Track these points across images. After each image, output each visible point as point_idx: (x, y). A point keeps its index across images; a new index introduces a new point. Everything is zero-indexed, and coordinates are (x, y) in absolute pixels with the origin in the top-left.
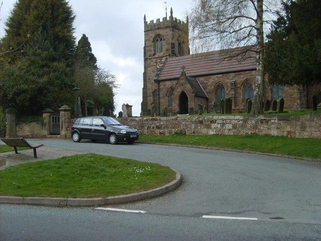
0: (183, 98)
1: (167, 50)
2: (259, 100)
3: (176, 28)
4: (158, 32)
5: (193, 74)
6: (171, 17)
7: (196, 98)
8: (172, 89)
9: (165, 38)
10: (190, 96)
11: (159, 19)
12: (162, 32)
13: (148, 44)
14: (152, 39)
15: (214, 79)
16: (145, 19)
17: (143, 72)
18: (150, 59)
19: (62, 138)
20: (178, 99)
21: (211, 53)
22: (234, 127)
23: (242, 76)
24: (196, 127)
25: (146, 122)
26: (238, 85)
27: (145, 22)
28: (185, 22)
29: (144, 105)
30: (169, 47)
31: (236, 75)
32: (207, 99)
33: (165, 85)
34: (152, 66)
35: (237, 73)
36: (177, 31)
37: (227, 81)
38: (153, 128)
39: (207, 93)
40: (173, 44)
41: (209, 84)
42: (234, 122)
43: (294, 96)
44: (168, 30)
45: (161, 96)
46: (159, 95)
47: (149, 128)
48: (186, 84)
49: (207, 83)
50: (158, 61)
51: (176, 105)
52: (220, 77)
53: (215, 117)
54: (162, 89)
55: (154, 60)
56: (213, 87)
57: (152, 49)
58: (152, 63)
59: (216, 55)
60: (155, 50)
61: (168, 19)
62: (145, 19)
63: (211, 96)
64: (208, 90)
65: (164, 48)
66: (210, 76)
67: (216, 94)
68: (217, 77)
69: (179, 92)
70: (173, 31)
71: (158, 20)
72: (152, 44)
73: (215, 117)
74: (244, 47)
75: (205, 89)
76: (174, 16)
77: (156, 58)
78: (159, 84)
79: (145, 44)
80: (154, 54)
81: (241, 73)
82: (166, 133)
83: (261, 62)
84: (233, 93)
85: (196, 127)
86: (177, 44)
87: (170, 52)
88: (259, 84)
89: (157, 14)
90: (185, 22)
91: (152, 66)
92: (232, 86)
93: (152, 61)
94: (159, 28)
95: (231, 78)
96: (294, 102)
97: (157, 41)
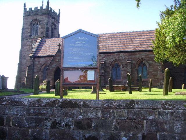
1: (42, 33)
4: (35, 17)
6: (48, 7)
11: (37, 8)
12: (38, 18)
13: (26, 26)
14: (29, 23)
16: (25, 6)
17: (20, 49)
23: (111, 57)
25: (49, 111)
26: (108, 65)
27: (25, 9)
28: (58, 13)
29: (19, 79)
33: (40, 61)
34: (28, 45)
36: (51, 18)
38: (67, 125)
40: (47, 28)
43: (157, 77)
44: (44, 16)
45: (35, 71)
46: (33, 70)
47: (55, 125)
50: (34, 41)
55: (30, 40)
57: (29, 31)
60: (31, 33)
61: (44, 8)
62: (25, 6)
65: (39, 32)
69: (54, 67)
70: (48, 17)
71: (36, 8)
72: (30, 27)
76: (50, 6)
79: (23, 26)
80: (30, 36)
81: (110, 54)
84: (103, 71)
86: (50, 29)
90: (58, 13)
93: (28, 41)
94: (36, 15)
96: (157, 82)
97: (34, 24)
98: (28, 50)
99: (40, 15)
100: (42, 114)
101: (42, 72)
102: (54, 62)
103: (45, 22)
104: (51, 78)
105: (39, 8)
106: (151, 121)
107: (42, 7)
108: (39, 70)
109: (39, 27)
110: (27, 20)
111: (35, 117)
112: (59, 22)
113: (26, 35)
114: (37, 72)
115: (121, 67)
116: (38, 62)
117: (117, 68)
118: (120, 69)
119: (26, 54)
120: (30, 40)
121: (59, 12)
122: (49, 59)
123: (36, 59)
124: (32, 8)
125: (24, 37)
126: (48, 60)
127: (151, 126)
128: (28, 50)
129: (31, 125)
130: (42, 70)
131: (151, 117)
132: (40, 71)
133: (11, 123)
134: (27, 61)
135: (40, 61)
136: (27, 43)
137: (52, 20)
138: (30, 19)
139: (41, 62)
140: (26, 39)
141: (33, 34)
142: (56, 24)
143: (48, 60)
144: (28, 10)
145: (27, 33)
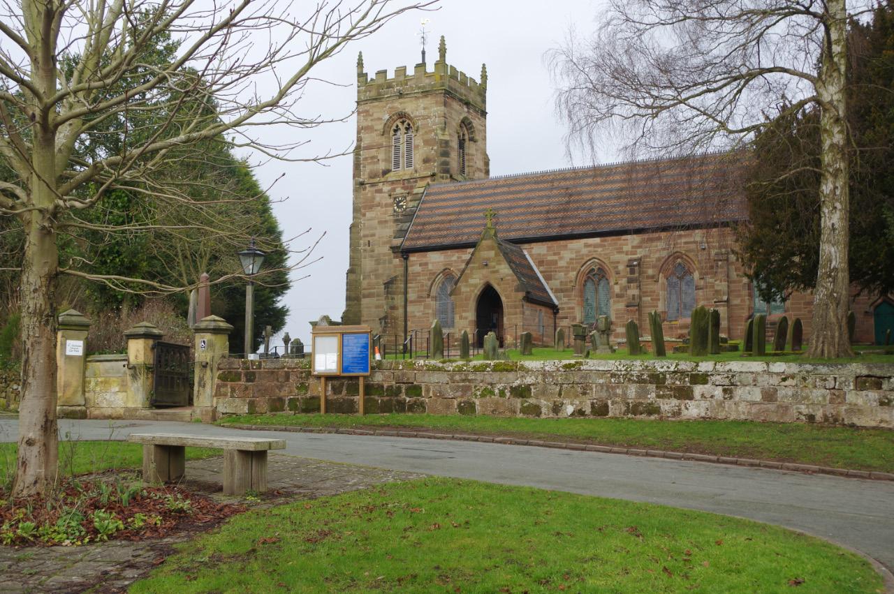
0: (489, 304)
1: (426, 161)
2: (836, 315)
3: (453, 98)
4: (399, 105)
5: (513, 235)
7: (526, 304)
8: (451, 279)
9: (420, 123)
10: (509, 297)
13: (368, 139)
15: (577, 252)
16: (360, 64)
17: (351, 222)
18: (373, 185)
19: (198, 421)
20: (472, 305)
21: (501, 183)
22: (769, 396)
23: (660, 245)
24: (643, 393)
25: (479, 376)
27: (362, 75)
28: (479, 81)
30: (433, 151)
31: (643, 241)
32: (554, 309)
33: (426, 264)
34: (379, 205)
35: (646, 236)
37: (616, 257)
38: (502, 393)
39: (556, 291)
41: (562, 263)
42: (766, 381)
46: (406, 293)
48: (499, 263)
49: (555, 262)
51: (465, 322)
52: (595, 246)
53: (705, 366)
54: (418, 274)
55: (386, 188)
56: (573, 274)
58: (378, 197)
59: (617, 177)
61: (430, 68)
62: (360, 64)
63: (565, 300)
64: (556, 283)
65: (417, 157)
66: (562, 243)
67: (582, 293)
68: (586, 246)
69: (475, 286)
70: (445, 104)
71: (401, 71)
73: (705, 366)
74: (631, 169)
75: (548, 278)
76: (449, 61)
77: (392, 182)
78: (406, 259)
79: (359, 140)
80: (386, 172)
82: (544, 410)
83: (838, 205)
85: (643, 393)
86: (455, 144)
87: (435, 167)
88: (835, 269)
89: (394, 50)
90: (479, 81)
91: (379, 205)
92: (632, 272)
93: (380, 191)
95: (625, 248)
98: (380, 222)
99: (417, 98)
100: (470, 381)
101: (435, 298)
102: (473, 268)
103: (435, 122)
104: (466, 318)
105: (411, 72)
106: (602, 385)
107: (421, 66)
108: (425, 294)
109: (418, 140)
110: (372, 115)
111: (461, 384)
112: (484, 114)
113: (369, 168)
114: (420, 300)
115: (696, 275)
116: (421, 265)
117: (681, 278)
118: (689, 283)
119: (373, 235)
120: (386, 188)
121: (484, 77)
122: (457, 255)
123: (413, 258)
124: (385, 72)
125: (364, 177)
126: (454, 258)
127: (601, 391)
128: (380, 222)
129: (457, 394)
130: (433, 293)
131: (601, 381)
132: (429, 296)
133: (843, 68)
134: (378, 262)
135: (426, 264)
136: (378, 199)
137: (459, 112)
138: (382, 113)
139: (430, 267)
140: (373, 185)
141: (397, 165)
142: (476, 123)
143: (454, 258)
144: (372, 75)
145: (374, 163)
